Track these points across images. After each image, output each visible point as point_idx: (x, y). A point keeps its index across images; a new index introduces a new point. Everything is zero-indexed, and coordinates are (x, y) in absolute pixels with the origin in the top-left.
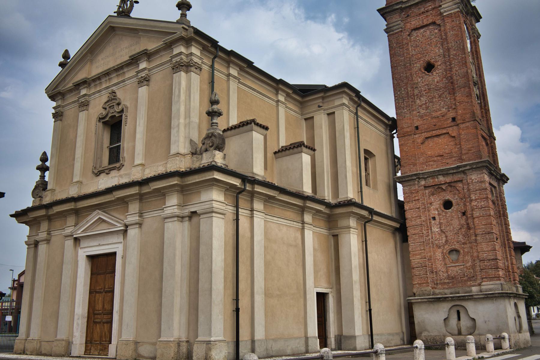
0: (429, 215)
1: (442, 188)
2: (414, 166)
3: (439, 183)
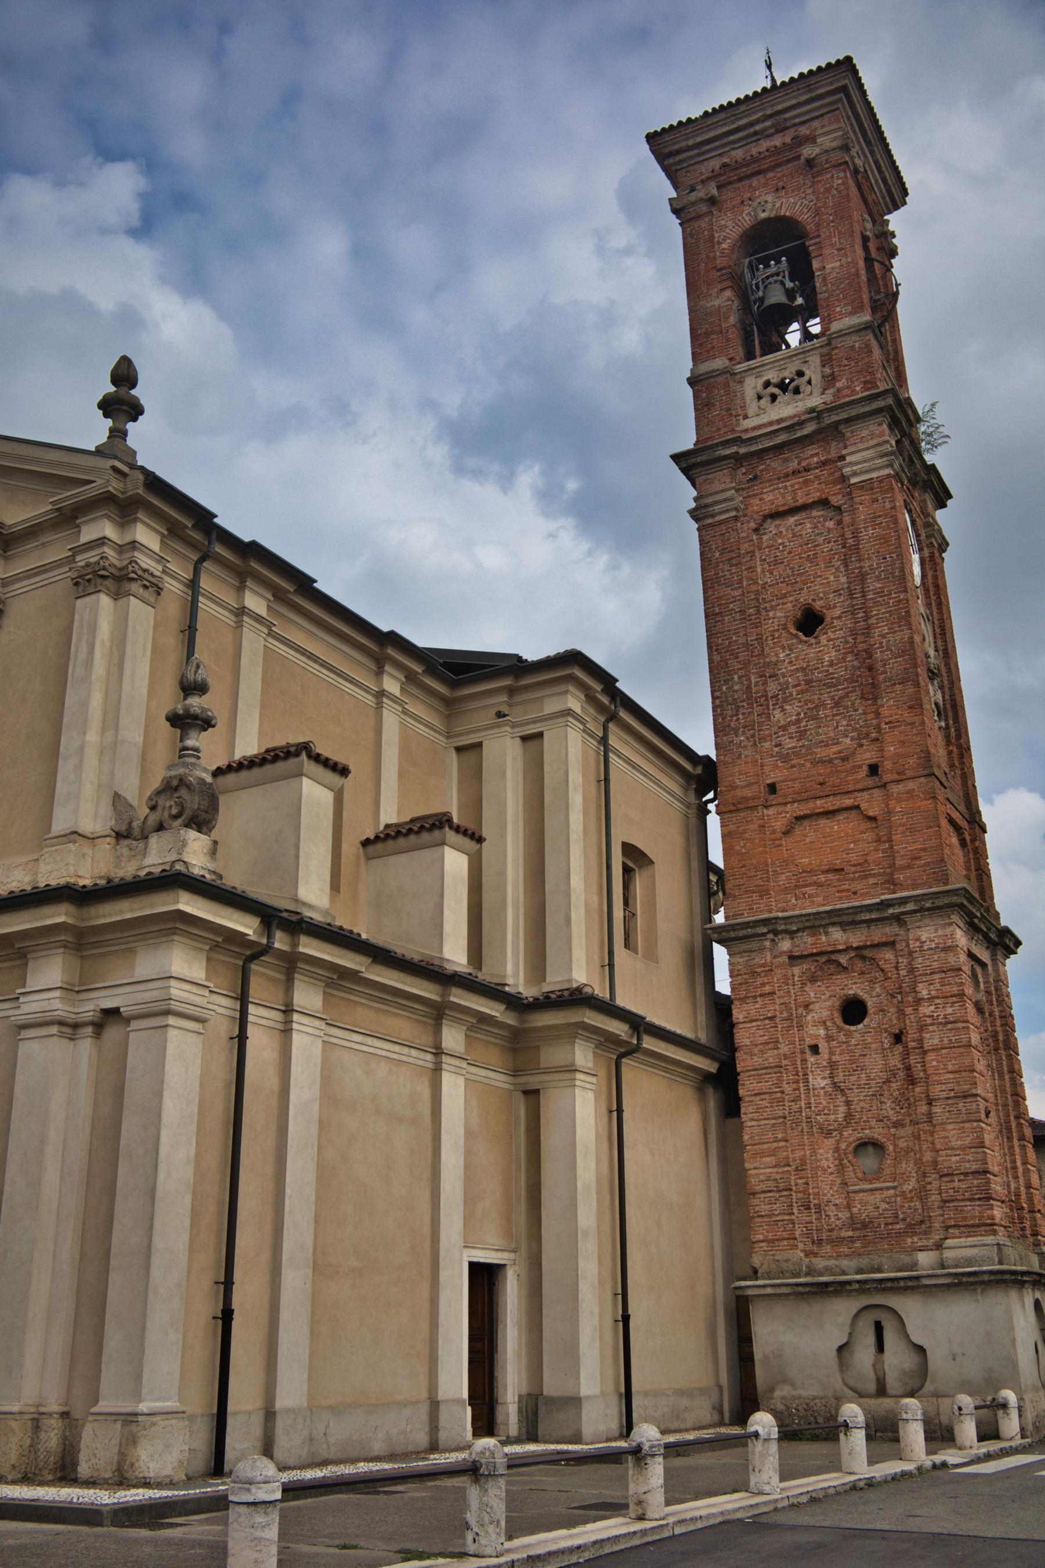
2: (761, 897)
3: (830, 949)
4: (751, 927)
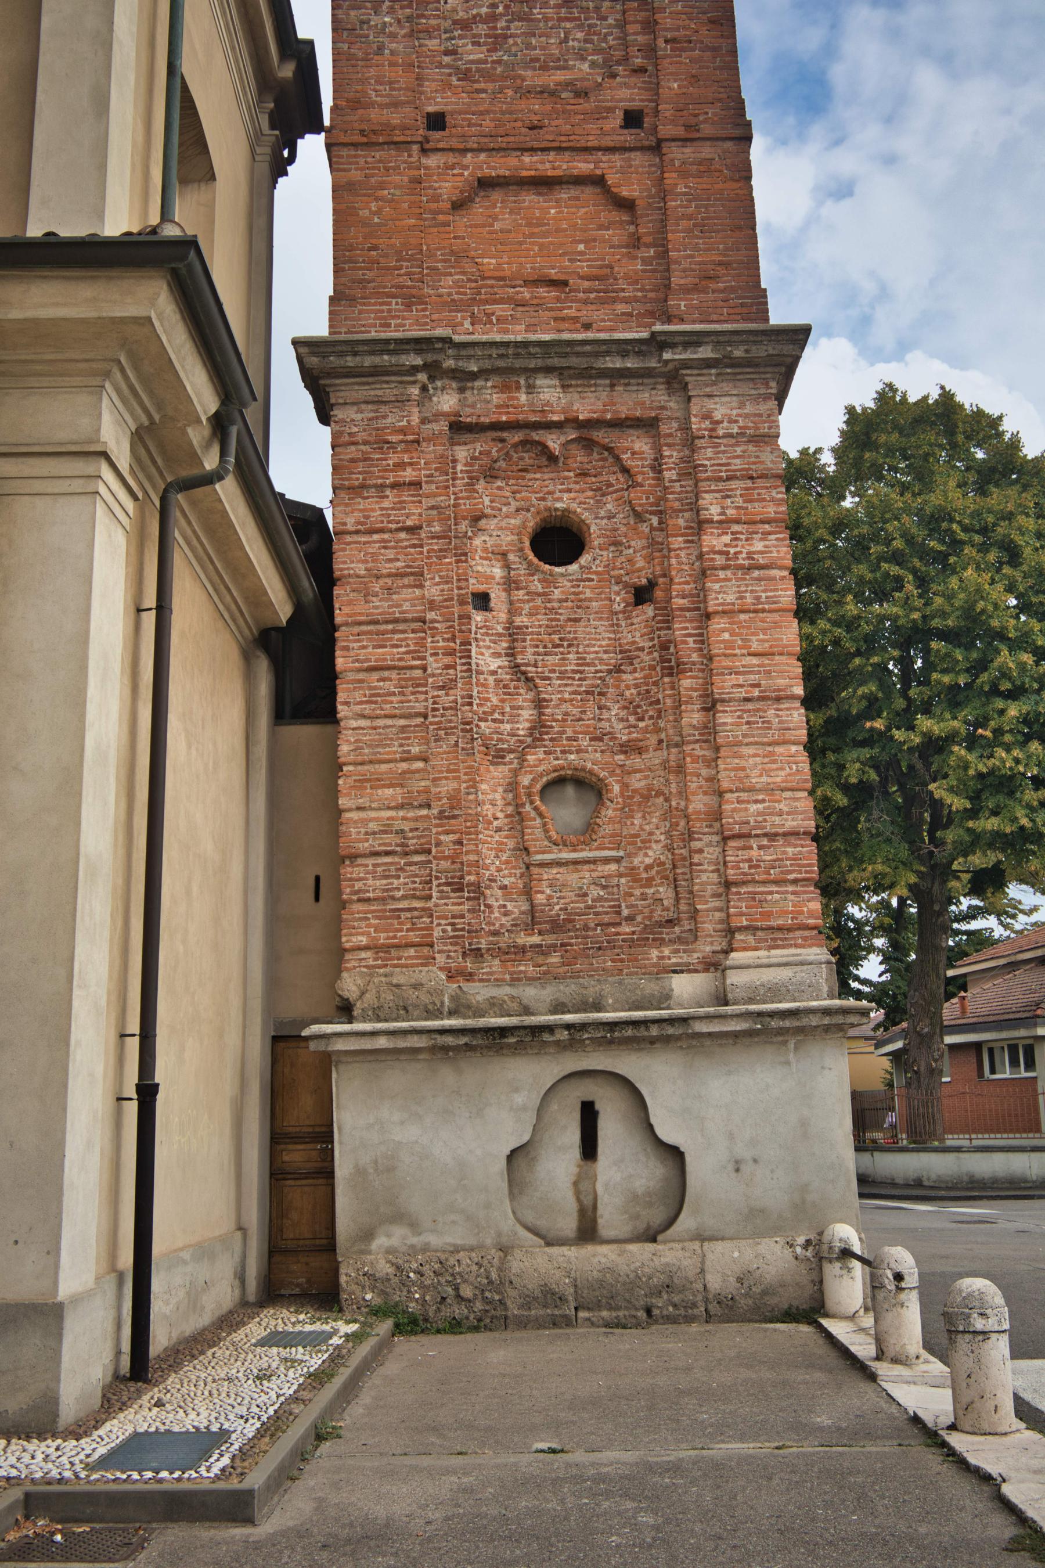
0: (463, 579)
1: (545, 447)
2: (408, 306)
3: (533, 418)
4: (390, 352)
